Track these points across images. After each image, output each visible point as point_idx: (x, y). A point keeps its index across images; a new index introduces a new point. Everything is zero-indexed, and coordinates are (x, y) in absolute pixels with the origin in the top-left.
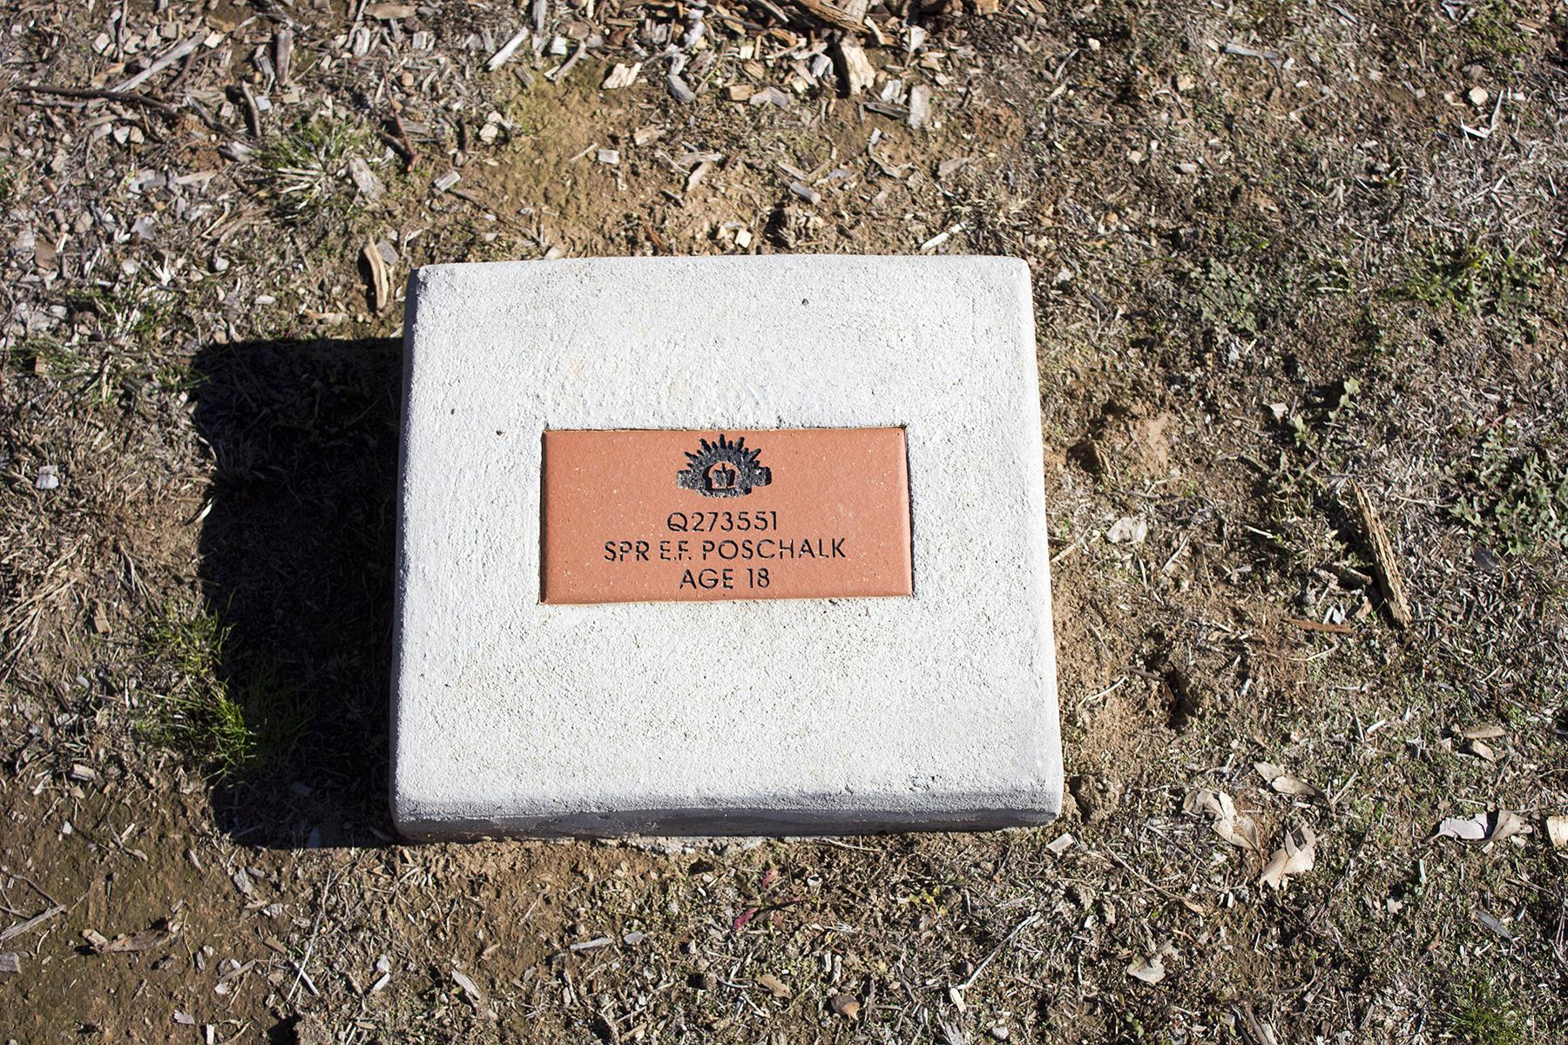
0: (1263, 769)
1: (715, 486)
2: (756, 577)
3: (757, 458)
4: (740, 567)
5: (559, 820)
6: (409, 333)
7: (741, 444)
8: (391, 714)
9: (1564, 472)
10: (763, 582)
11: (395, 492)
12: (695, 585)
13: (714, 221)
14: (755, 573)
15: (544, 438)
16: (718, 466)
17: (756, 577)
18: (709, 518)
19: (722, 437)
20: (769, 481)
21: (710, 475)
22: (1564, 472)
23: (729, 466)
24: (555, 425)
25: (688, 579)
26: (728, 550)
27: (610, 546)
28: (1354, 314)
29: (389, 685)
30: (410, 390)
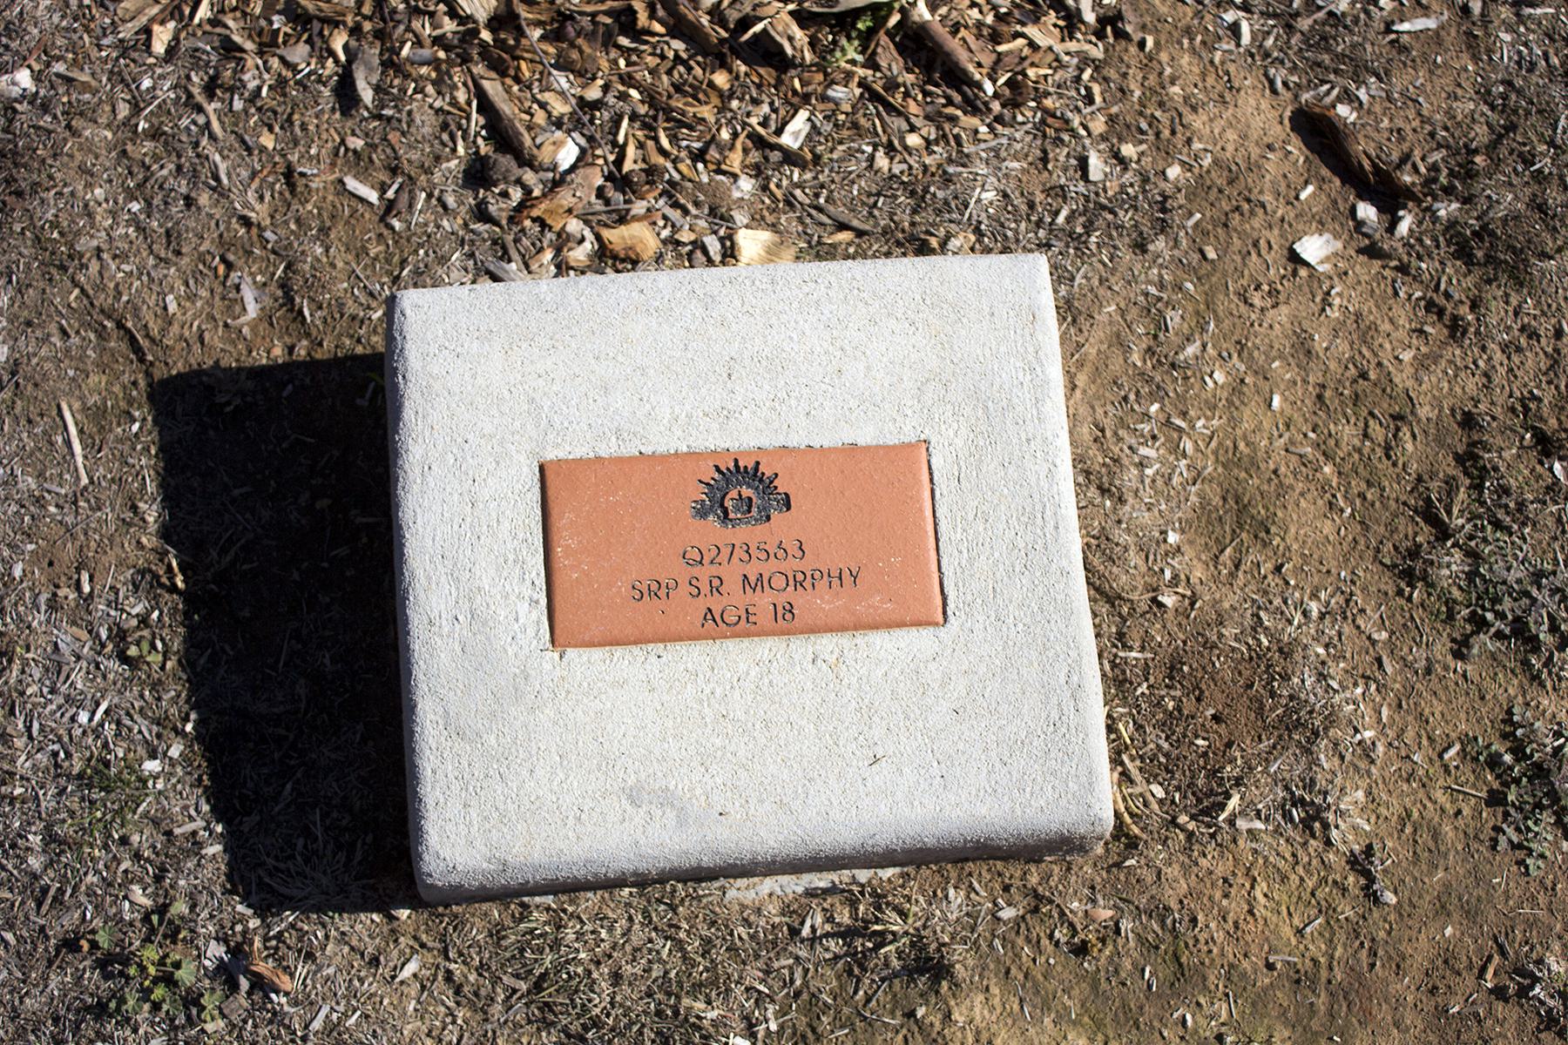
0: (1207, 743)
1: (732, 515)
2: (780, 611)
3: (775, 483)
4: (763, 602)
5: (851, 858)
6: (390, 338)
7: (756, 469)
8: (411, 826)
9: (1320, 8)
10: (788, 616)
11: (410, 863)
12: (716, 625)
13: (709, 165)
14: (780, 609)
15: (542, 468)
16: (734, 494)
17: (780, 611)
18: (726, 551)
19: (736, 461)
20: (789, 508)
21: (728, 504)
22: (1320, 8)
23: (747, 492)
24: (550, 455)
25: (709, 616)
26: (779, 582)
27: (694, 582)
28: (1256, 237)
29: (400, 698)
30: (406, 622)
